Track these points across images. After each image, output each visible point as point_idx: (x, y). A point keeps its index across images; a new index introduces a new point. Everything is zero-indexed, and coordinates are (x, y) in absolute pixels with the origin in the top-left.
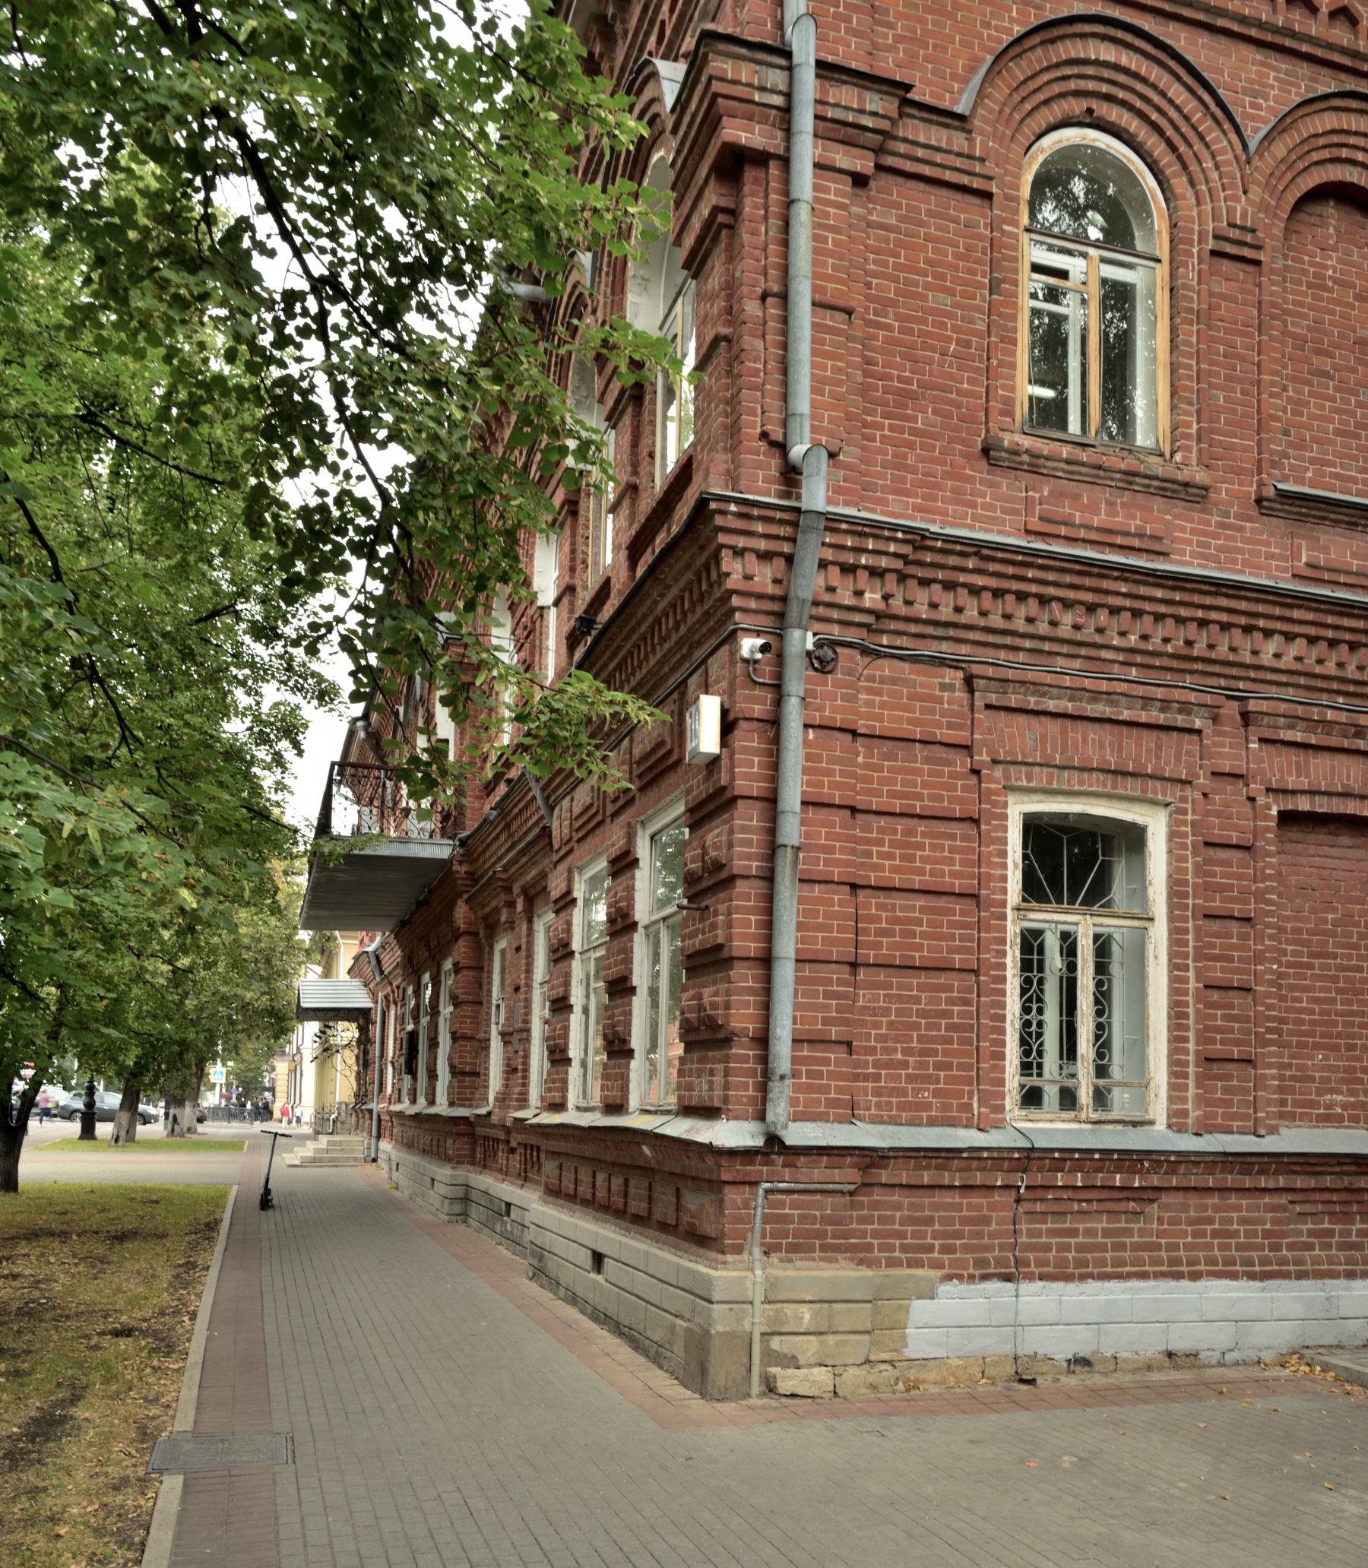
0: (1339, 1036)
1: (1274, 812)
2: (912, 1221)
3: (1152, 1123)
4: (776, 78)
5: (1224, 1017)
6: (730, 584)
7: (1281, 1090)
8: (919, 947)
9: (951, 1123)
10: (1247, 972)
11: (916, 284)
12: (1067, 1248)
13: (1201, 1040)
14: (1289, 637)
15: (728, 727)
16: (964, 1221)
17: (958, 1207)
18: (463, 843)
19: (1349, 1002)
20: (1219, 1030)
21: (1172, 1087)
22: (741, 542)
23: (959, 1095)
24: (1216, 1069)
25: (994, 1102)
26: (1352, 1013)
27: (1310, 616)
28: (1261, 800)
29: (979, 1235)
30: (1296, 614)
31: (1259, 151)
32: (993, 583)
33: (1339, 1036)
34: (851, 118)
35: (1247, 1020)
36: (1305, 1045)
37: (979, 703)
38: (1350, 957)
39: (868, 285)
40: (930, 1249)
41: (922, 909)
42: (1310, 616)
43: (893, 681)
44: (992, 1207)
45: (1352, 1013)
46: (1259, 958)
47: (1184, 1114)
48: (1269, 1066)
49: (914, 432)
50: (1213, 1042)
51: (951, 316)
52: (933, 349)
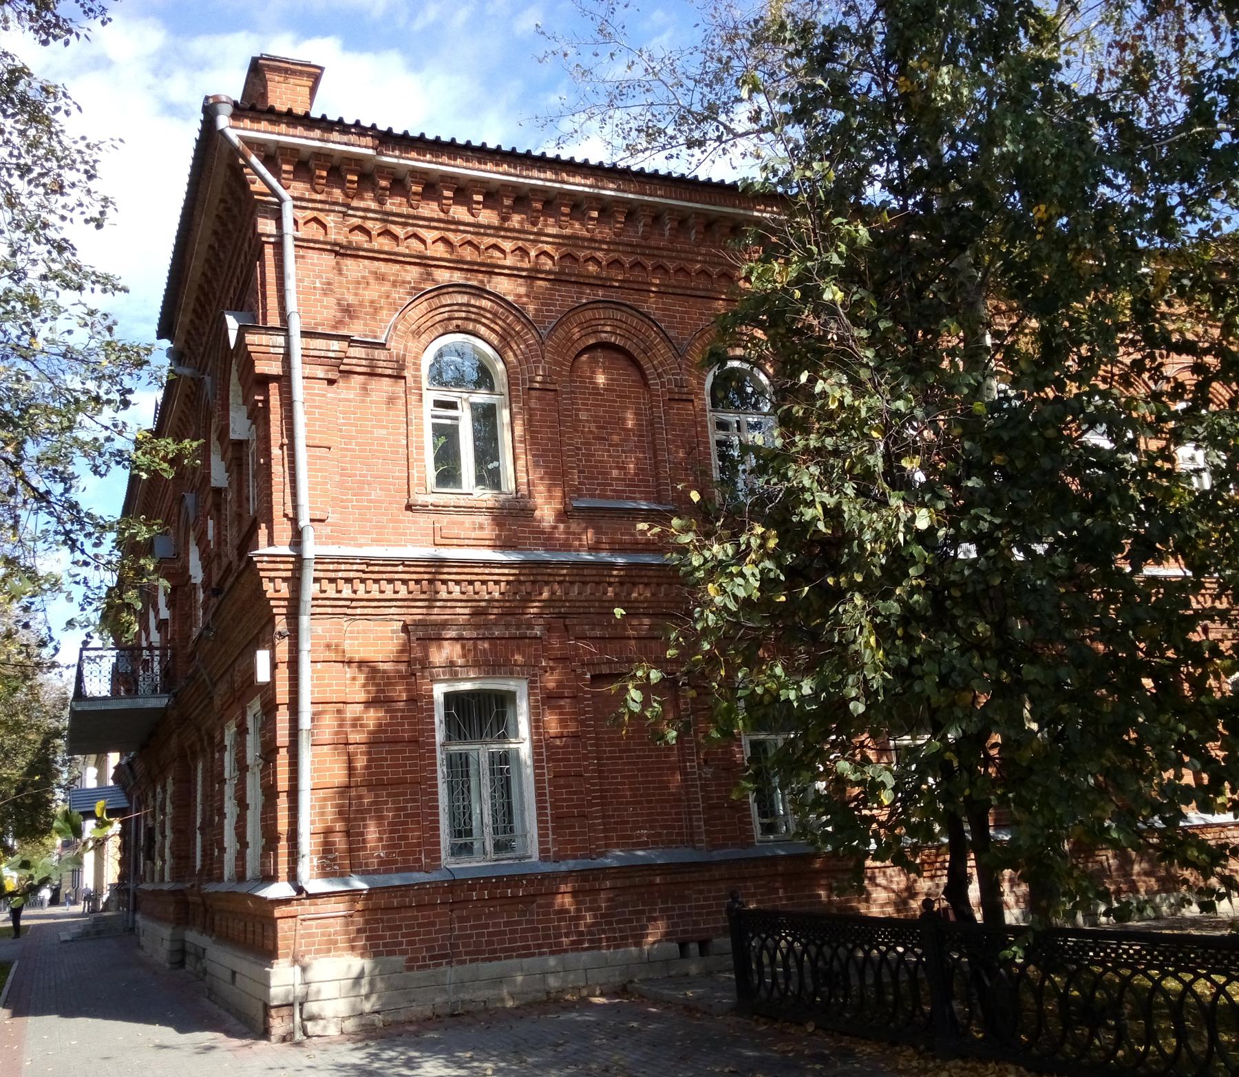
0: (641, 796)
1: (588, 676)
2: (390, 928)
3: (530, 857)
4: (281, 340)
5: (567, 793)
6: (268, 595)
7: (604, 831)
8: (386, 773)
9: (410, 869)
10: (580, 766)
11: (366, 426)
12: (482, 935)
13: (553, 807)
14: (584, 583)
15: (274, 666)
16: (419, 926)
17: (416, 918)
18: (175, 695)
19: (646, 776)
20: (564, 800)
21: (540, 836)
22: (272, 574)
23: (414, 853)
24: (565, 822)
25: (434, 855)
26: (650, 782)
27: (594, 572)
28: (579, 671)
29: (429, 933)
30: (586, 572)
31: (549, 337)
32: (415, 576)
33: (641, 796)
34: (323, 354)
35: (582, 793)
36: (621, 803)
37: (413, 638)
38: (644, 750)
39: (341, 430)
40: (401, 943)
41: (388, 752)
42: (594, 572)
43: (365, 632)
44: (437, 915)
45: (650, 782)
46: (585, 758)
47: (548, 850)
48: (596, 818)
49: (371, 501)
50: (712, 798)
51: (387, 440)
52: (378, 458)
